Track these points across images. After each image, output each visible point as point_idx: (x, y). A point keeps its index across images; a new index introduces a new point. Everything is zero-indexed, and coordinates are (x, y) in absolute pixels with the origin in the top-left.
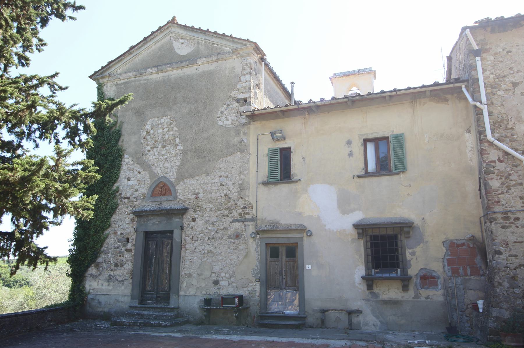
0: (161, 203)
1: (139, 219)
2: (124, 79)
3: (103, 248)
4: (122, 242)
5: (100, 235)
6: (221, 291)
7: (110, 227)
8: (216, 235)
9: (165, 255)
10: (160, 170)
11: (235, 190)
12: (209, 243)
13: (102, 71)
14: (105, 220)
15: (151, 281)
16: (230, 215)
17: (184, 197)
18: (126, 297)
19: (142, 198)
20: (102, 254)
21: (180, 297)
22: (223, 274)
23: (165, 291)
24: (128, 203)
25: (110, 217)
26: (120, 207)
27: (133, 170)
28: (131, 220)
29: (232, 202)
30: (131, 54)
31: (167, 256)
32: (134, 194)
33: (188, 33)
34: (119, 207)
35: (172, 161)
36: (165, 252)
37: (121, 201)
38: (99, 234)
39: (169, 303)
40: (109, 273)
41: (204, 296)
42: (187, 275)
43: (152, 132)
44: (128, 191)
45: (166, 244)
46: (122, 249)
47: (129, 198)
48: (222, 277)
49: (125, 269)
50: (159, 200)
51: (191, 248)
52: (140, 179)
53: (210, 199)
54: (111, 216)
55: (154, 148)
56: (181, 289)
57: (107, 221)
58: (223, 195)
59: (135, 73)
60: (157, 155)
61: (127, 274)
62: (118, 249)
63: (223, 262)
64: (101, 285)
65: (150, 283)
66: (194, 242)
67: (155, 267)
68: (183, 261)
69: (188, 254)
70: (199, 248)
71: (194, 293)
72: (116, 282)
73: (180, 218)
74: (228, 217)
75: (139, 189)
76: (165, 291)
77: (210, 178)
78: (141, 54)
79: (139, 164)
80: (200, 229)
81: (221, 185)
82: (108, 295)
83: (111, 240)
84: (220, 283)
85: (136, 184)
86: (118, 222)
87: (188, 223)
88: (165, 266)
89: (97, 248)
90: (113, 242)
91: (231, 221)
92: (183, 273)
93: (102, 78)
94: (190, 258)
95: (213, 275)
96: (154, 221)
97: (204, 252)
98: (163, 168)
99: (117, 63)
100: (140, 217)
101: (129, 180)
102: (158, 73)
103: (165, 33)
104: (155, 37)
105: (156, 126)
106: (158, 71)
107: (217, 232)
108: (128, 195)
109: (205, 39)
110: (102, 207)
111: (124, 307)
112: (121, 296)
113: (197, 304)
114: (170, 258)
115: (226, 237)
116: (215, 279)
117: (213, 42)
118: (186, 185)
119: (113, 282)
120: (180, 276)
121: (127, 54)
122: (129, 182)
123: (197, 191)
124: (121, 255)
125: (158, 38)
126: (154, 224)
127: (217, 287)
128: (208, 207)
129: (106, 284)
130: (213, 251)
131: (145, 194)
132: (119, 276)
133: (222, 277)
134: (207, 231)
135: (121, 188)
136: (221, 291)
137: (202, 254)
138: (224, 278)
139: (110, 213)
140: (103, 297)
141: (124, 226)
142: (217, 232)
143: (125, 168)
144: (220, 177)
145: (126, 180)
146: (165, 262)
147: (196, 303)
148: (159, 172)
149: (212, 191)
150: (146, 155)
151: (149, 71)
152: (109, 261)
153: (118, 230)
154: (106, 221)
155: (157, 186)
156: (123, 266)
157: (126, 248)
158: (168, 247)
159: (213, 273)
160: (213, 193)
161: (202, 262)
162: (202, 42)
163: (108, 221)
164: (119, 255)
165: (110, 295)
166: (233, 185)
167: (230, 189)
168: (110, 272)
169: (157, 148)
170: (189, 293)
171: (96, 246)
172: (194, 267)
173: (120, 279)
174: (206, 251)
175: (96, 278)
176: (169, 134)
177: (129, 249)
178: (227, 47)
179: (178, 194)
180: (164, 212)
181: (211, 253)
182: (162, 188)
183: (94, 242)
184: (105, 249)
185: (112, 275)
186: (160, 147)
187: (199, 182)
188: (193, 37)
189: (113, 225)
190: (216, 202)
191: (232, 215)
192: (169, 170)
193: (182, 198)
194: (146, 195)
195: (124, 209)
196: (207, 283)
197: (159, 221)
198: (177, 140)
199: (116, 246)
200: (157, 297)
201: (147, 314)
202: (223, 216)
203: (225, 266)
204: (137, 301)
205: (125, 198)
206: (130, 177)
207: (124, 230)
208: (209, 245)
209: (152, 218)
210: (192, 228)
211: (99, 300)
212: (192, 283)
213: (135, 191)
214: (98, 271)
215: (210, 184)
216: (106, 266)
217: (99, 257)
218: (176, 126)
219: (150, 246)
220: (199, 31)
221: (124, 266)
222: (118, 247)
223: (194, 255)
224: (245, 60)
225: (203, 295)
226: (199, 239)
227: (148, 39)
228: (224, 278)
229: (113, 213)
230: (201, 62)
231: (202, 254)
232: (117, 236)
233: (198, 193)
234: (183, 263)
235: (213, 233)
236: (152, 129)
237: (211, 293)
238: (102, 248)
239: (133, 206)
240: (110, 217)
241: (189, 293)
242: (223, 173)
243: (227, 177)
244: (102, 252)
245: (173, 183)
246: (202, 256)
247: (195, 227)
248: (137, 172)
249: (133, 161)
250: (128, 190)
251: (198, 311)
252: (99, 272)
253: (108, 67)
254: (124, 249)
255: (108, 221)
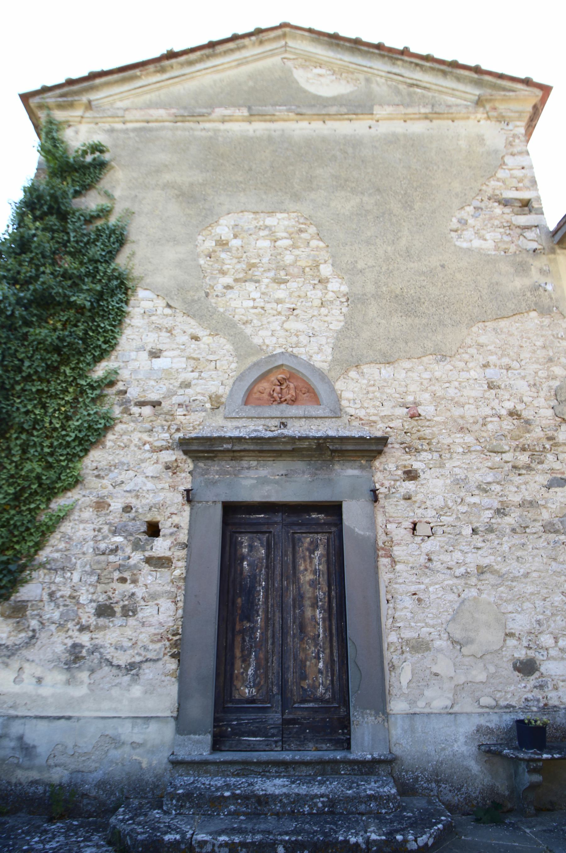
0: (284, 425)
1: (201, 464)
2: (137, 121)
3: (43, 556)
4: (131, 535)
5: (38, 508)
6: (550, 695)
7: (79, 486)
8: (499, 520)
9: (307, 578)
10: (272, 335)
11: (541, 402)
12: (479, 545)
13: (65, 89)
14: (59, 461)
15: (253, 664)
16: (539, 467)
17: (368, 411)
18: (153, 727)
19: (208, 406)
20: (42, 572)
21: (392, 719)
22: (546, 640)
23: (315, 700)
24: (154, 418)
25: (82, 454)
26: (119, 428)
27: (170, 331)
28: (168, 468)
29: (537, 433)
30: (163, 70)
31: (313, 584)
32: (176, 394)
33: (339, 56)
34: (117, 428)
35: (314, 316)
36: (306, 570)
37: (126, 411)
38: (32, 506)
39: (347, 745)
40: (71, 637)
41: (488, 714)
42: (407, 644)
43: (235, 243)
44: (153, 386)
45: (306, 545)
46: (129, 558)
47: (156, 404)
48: (547, 649)
49: (143, 624)
50: (278, 414)
51: (411, 559)
52: (199, 356)
53: (461, 422)
54: (86, 451)
55: (246, 281)
56: (394, 691)
57: (67, 467)
58: (504, 412)
59: (173, 111)
60: (258, 300)
61: (152, 641)
62: (112, 558)
63: (539, 603)
64: (34, 680)
65: (250, 672)
66: (423, 540)
67: (267, 619)
68: (389, 597)
69: (405, 574)
70: (441, 557)
71: (449, 703)
72: (107, 669)
73: (362, 467)
74: (531, 470)
75: (193, 382)
76: (315, 700)
77: (449, 367)
78: (193, 78)
79: (194, 317)
80: (439, 502)
81: (491, 386)
82: (69, 718)
83: (82, 526)
84: (542, 669)
85: (185, 369)
86: (110, 470)
87: (393, 483)
88: (309, 613)
89: (19, 552)
90: (92, 534)
91: (546, 483)
92: (391, 638)
93: (61, 107)
94: (413, 589)
95: (511, 642)
96: (263, 472)
97: (462, 570)
98: (282, 333)
99: (116, 82)
100: (208, 458)
101: (155, 354)
102: (249, 119)
103: (268, 47)
104: (239, 49)
105: (250, 232)
106: (251, 115)
107: (500, 512)
108: (154, 397)
109: (389, 73)
110: (51, 423)
111: (144, 765)
112: (128, 724)
113: (466, 743)
114: (326, 589)
115: (537, 527)
116: (521, 654)
117: (415, 82)
118: (369, 380)
119: (92, 671)
120: (385, 646)
121: (151, 68)
122: (154, 360)
123: (410, 398)
124: (127, 575)
125: (244, 53)
126: (263, 481)
127: (532, 681)
128: (457, 441)
129: (60, 677)
130: (496, 567)
131: (218, 397)
132: (118, 647)
133: (547, 649)
134: (463, 509)
135: (125, 374)
136: (552, 694)
137: (456, 577)
138: (552, 653)
139: (80, 441)
140: (42, 725)
141: (136, 485)
142: (500, 512)
143: (139, 325)
144: (486, 366)
145: (144, 355)
146: (307, 603)
147: (462, 739)
148: (271, 341)
149: (462, 400)
150: (217, 296)
151: (219, 112)
152: (72, 597)
153: (110, 495)
154: (64, 464)
155: (263, 377)
156: (135, 612)
157: (147, 554)
158: (318, 553)
159: (511, 635)
160: (467, 407)
161: (463, 602)
162: (378, 79)
163: (71, 465)
164: (116, 575)
165: (79, 719)
166: (533, 389)
167: (525, 399)
168: (77, 633)
169: (257, 281)
170: (428, 704)
171: (18, 542)
172: (433, 619)
173: (122, 659)
174: (472, 569)
175: (9, 657)
176: (296, 252)
177: (160, 558)
178: (453, 96)
179: (344, 403)
180: (306, 444)
181: (491, 572)
182: (281, 384)
183: (11, 532)
184: (56, 555)
185: (83, 647)
186: (266, 281)
187: (415, 375)
188: (354, 66)
189: (90, 480)
190: (483, 429)
191: (544, 466)
192: (303, 339)
193: (362, 413)
194: (223, 400)
195: (136, 437)
196: (492, 669)
197: (284, 472)
198: (326, 270)
199: (103, 546)
200: (286, 722)
201: (287, 796)
202: (514, 467)
203: (548, 613)
204: (209, 738)
205: (141, 404)
206: (160, 347)
207: (137, 497)
208: (478, 549)
209: (254, 463)
210: (408, 498)
211: (21, 738)
212: (435, 669)
213: (180, 387)
214: (20, 631)
215: (456, 384)
216: (56, 615)
217: (27, 582)
218: (319, 236)
219: (245, 550)
220: (376, 51)
221: (140, 615)
222: (115, 551)
223: (427, 581)
224: (510, 127)
225: (487, 710)
226: (439, 531)
227: (220, 49)
228: (552, 653)
229: (92, 444)
230: (384, 113)
231: (456, 577)
232: (108, 514)
233: (417, 404)
234: (391, 605)
235: (489, 514)
236: (235, 236)
237: (514, 704)
238: (41, 553)
239: (175, 427)
240: (82, 454)
241: (428, 704)
242: (493, 359)
243: (507, 370)
244: (42, 565)
245: (326, 372)
246: (455, 581)
247: (419, 497)
248: (187, 337)
249: (169, 306)
250: (152, 383)
251: (475, 767)
252: (23, 635)
253: (85, 84)
254: (137, 557)
255: (71, 465)
